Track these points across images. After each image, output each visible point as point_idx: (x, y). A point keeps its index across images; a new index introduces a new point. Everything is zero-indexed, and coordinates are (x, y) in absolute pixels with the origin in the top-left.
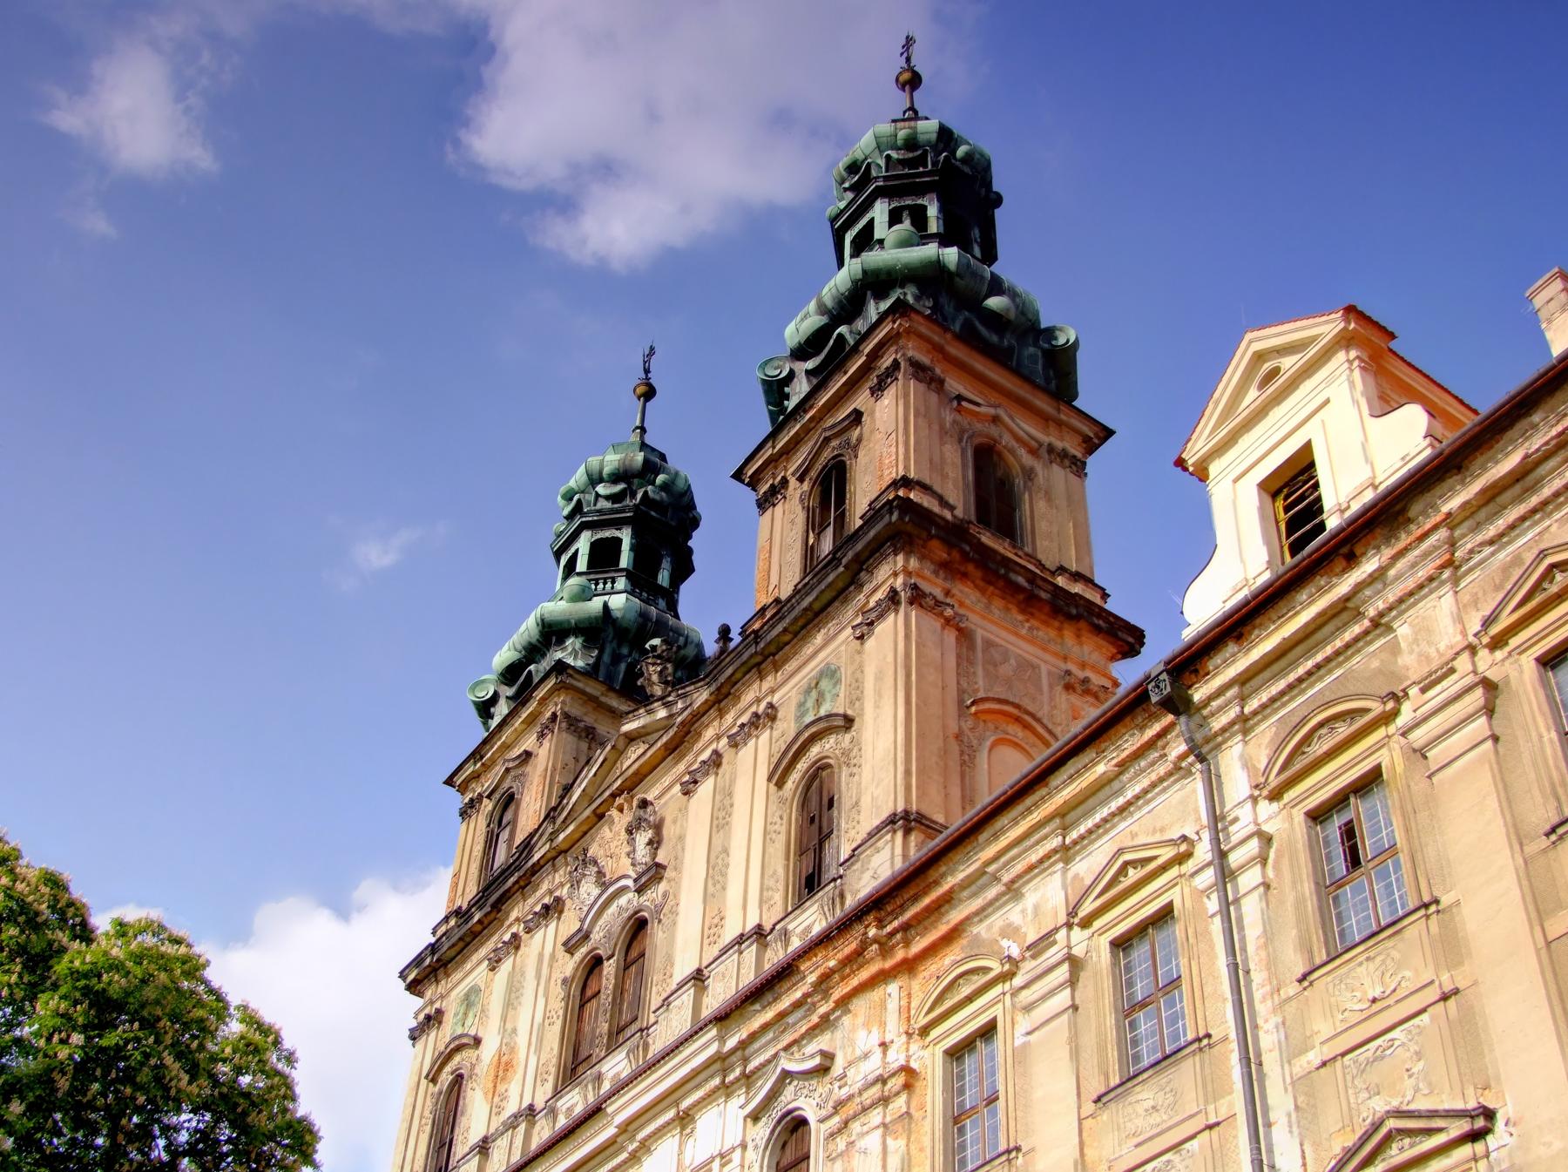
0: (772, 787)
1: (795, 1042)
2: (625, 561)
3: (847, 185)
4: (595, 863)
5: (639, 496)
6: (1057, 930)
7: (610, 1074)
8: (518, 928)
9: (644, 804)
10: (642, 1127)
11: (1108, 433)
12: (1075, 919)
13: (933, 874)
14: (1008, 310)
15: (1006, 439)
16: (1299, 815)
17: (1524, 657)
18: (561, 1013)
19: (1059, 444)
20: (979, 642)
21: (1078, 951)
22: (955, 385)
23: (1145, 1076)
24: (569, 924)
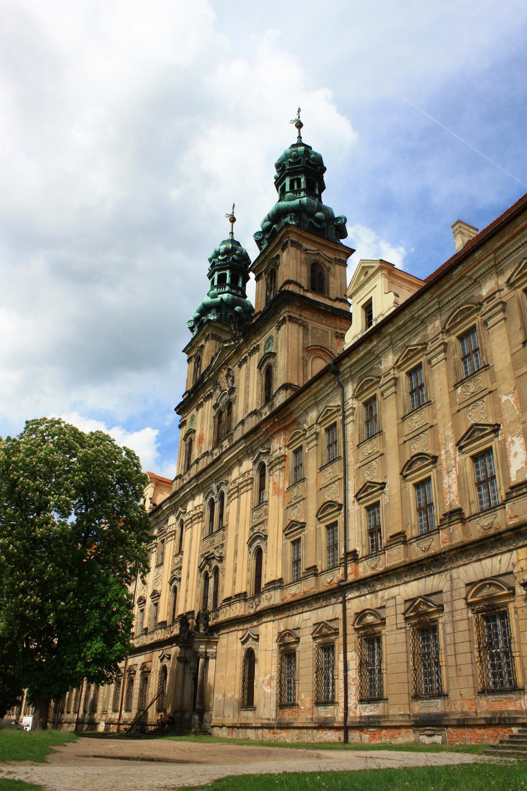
2: (228, 281)
4: (219, 384)
5: (231, 259)
9: (229, 370)
10: (231, 462)
11: (353, 251)
14: (322, 217)
15: (322, 260)
16: (361, 403)
19: (338, 257)
20: (310, 328)
22: (305, 246)
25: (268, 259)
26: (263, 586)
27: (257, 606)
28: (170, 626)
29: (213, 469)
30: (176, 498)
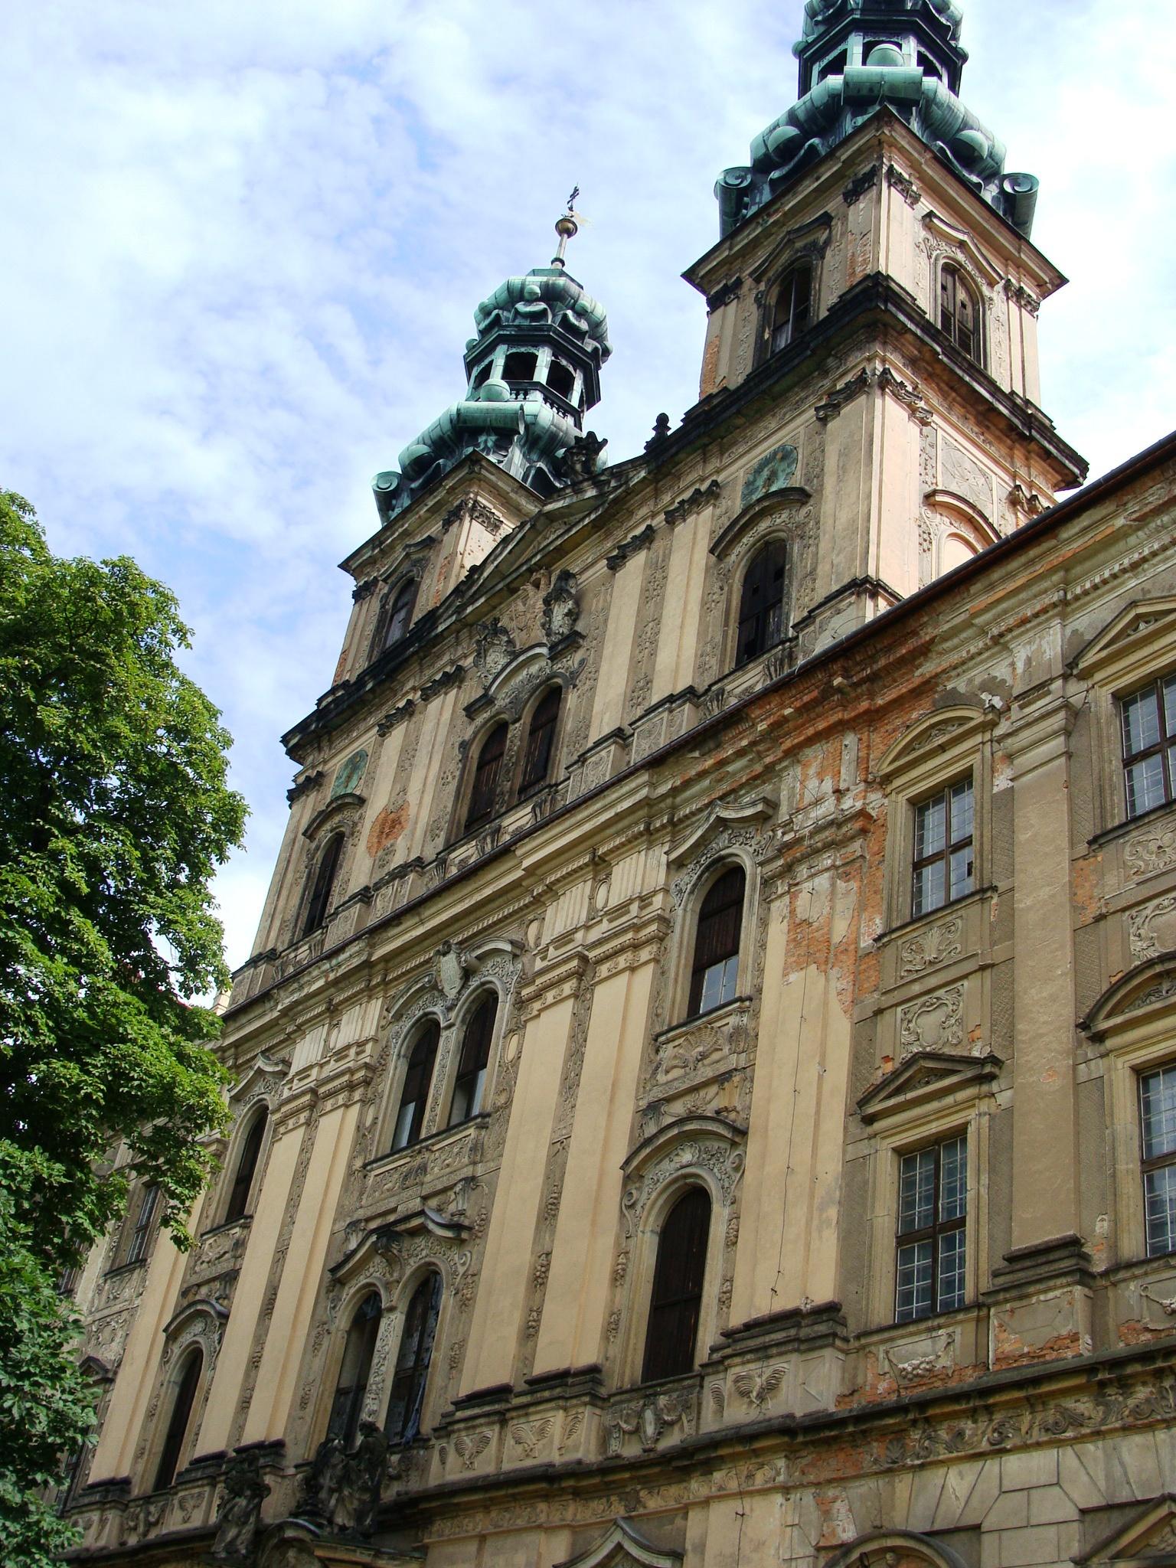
0: (713, 559)
1: (733, 791)
2: (541, 375)
3: (820, 18)
6: (1052, 680)
7: (511, 829)
8: (659, 521)
9: (566, 576)
10: (551, 871)
12: (1072, 668)
13: (913, 624)
18: (458, 773)
21: (1076, 701)
23: (1152, 817)
24: (471, 691)
26: (708, 1336)
27: (150, 1525)
28: (147, 1500)
29: (461, 900)
30: (250, 1022)
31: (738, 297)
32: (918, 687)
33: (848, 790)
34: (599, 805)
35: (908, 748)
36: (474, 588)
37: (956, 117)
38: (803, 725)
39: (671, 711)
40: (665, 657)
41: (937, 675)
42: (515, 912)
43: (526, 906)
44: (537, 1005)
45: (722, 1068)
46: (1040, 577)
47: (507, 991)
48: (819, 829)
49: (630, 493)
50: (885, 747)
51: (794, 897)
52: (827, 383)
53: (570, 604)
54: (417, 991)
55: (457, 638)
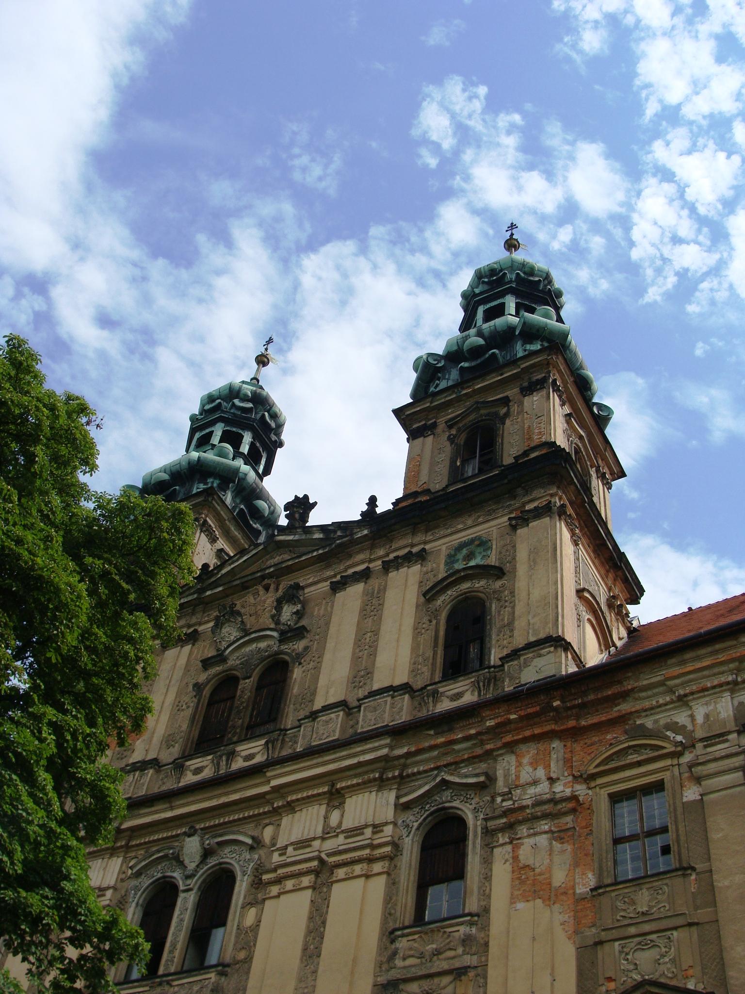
1: (456, 763)
8: (377, 565)
17: (603, 790)
25: (476, 398)
31: (434, 434)
32: (616, 718)
33: (558, 779)
34: (344, 753)
35: (609, 759)
36: (213, 579)
37: (577, 360)
38: (522, 728)
39: (393, 697)
40: (383, 659)
41: (631, 713)
42: (254, 816)
43: (265, 813)
44: (275, 890)
45: (457, 964)
46: (722, 663)
47: (244, 873)
48: (538, 803)
49: (354, 542)
50: (591, 754)
51: (516, 848)
52: (517, 504)
53: (299, 607)
54: (157, 858)
55: (194, 610)
